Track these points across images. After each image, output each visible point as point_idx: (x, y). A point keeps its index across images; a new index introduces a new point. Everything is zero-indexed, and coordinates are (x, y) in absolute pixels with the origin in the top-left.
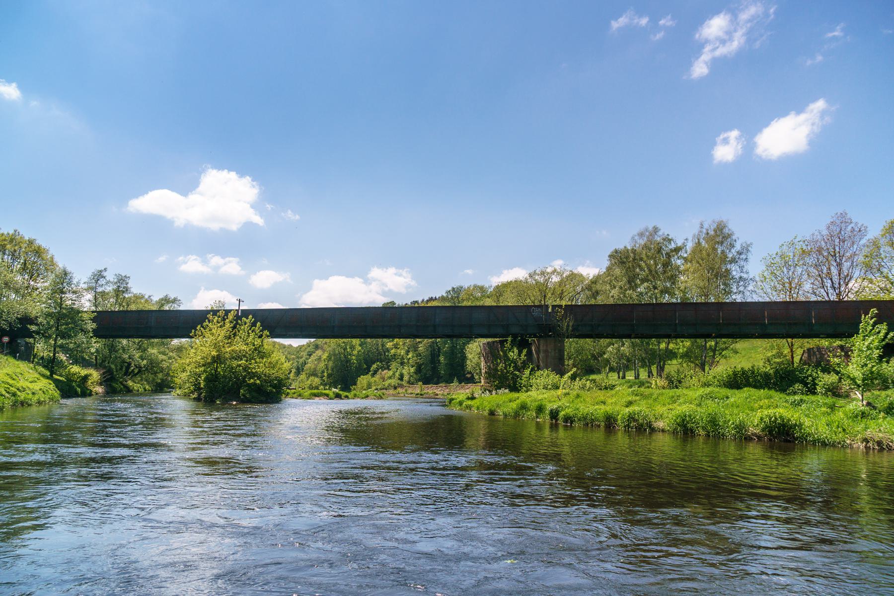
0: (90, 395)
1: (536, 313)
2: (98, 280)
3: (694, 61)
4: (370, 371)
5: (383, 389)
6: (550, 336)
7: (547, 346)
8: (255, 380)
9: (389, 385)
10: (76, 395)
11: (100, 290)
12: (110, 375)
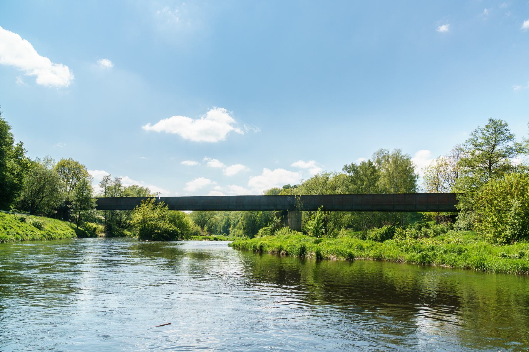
0: (96, 236)
1: (289, 199)
11: (107, 185)
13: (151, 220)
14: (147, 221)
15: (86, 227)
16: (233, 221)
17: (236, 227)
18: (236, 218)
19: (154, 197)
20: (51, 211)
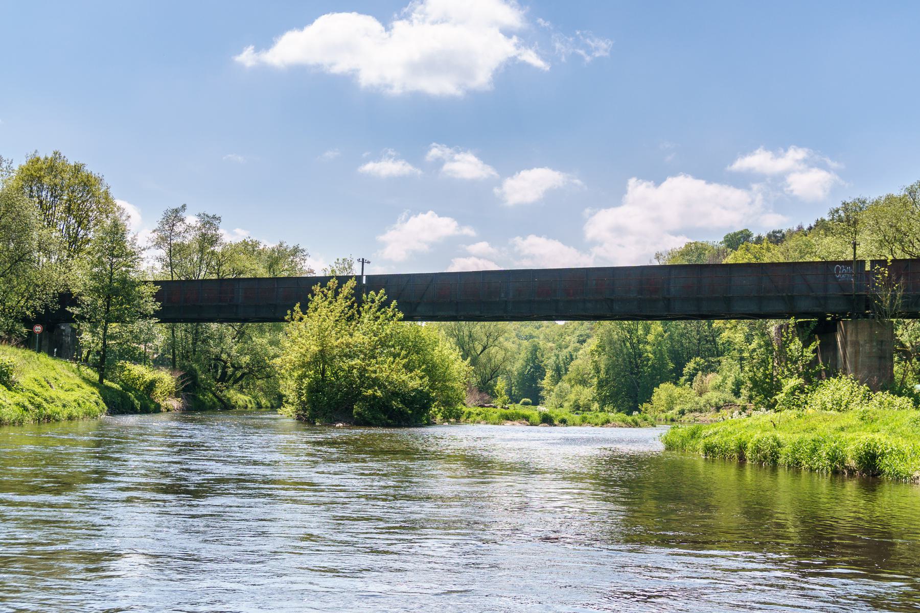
0: (157, 410)
1: (843, 275)
2: (173, 225)
3: (390, 157)
4: (682, 375)
5: (696, 410)
6: (866, 316)
7: (857, 336)
8: (375, 391)
9: (708, 402)
10: (133, 411)
12: (191, 379)
13: (346, 355)
14: (332, 359)
15: (123, 377)
16: (554, 358)
17: (565, 377)
18: (560, 347)
19: (351, 277)
20: (13, 326)
